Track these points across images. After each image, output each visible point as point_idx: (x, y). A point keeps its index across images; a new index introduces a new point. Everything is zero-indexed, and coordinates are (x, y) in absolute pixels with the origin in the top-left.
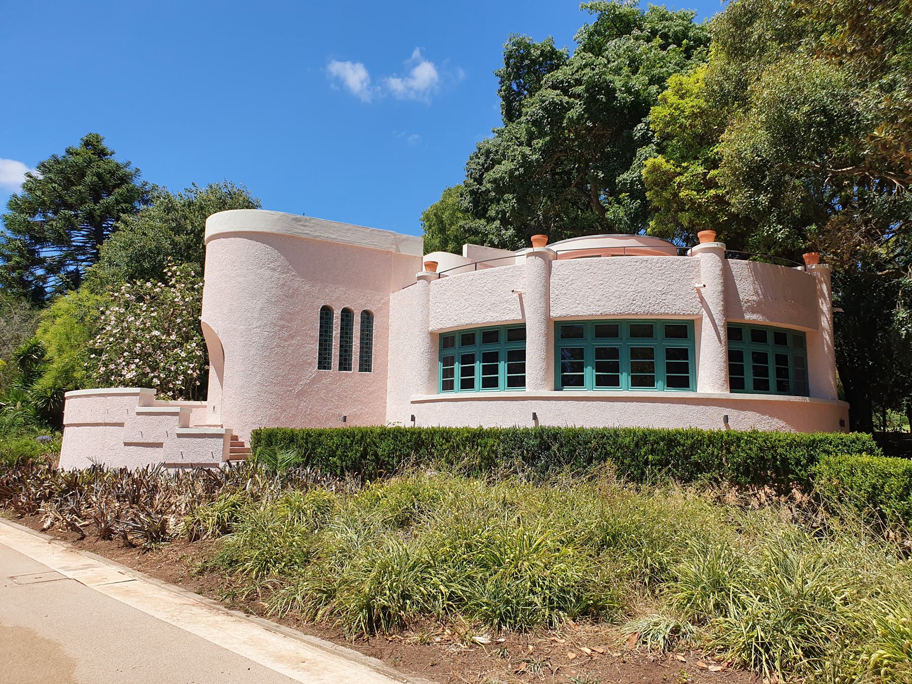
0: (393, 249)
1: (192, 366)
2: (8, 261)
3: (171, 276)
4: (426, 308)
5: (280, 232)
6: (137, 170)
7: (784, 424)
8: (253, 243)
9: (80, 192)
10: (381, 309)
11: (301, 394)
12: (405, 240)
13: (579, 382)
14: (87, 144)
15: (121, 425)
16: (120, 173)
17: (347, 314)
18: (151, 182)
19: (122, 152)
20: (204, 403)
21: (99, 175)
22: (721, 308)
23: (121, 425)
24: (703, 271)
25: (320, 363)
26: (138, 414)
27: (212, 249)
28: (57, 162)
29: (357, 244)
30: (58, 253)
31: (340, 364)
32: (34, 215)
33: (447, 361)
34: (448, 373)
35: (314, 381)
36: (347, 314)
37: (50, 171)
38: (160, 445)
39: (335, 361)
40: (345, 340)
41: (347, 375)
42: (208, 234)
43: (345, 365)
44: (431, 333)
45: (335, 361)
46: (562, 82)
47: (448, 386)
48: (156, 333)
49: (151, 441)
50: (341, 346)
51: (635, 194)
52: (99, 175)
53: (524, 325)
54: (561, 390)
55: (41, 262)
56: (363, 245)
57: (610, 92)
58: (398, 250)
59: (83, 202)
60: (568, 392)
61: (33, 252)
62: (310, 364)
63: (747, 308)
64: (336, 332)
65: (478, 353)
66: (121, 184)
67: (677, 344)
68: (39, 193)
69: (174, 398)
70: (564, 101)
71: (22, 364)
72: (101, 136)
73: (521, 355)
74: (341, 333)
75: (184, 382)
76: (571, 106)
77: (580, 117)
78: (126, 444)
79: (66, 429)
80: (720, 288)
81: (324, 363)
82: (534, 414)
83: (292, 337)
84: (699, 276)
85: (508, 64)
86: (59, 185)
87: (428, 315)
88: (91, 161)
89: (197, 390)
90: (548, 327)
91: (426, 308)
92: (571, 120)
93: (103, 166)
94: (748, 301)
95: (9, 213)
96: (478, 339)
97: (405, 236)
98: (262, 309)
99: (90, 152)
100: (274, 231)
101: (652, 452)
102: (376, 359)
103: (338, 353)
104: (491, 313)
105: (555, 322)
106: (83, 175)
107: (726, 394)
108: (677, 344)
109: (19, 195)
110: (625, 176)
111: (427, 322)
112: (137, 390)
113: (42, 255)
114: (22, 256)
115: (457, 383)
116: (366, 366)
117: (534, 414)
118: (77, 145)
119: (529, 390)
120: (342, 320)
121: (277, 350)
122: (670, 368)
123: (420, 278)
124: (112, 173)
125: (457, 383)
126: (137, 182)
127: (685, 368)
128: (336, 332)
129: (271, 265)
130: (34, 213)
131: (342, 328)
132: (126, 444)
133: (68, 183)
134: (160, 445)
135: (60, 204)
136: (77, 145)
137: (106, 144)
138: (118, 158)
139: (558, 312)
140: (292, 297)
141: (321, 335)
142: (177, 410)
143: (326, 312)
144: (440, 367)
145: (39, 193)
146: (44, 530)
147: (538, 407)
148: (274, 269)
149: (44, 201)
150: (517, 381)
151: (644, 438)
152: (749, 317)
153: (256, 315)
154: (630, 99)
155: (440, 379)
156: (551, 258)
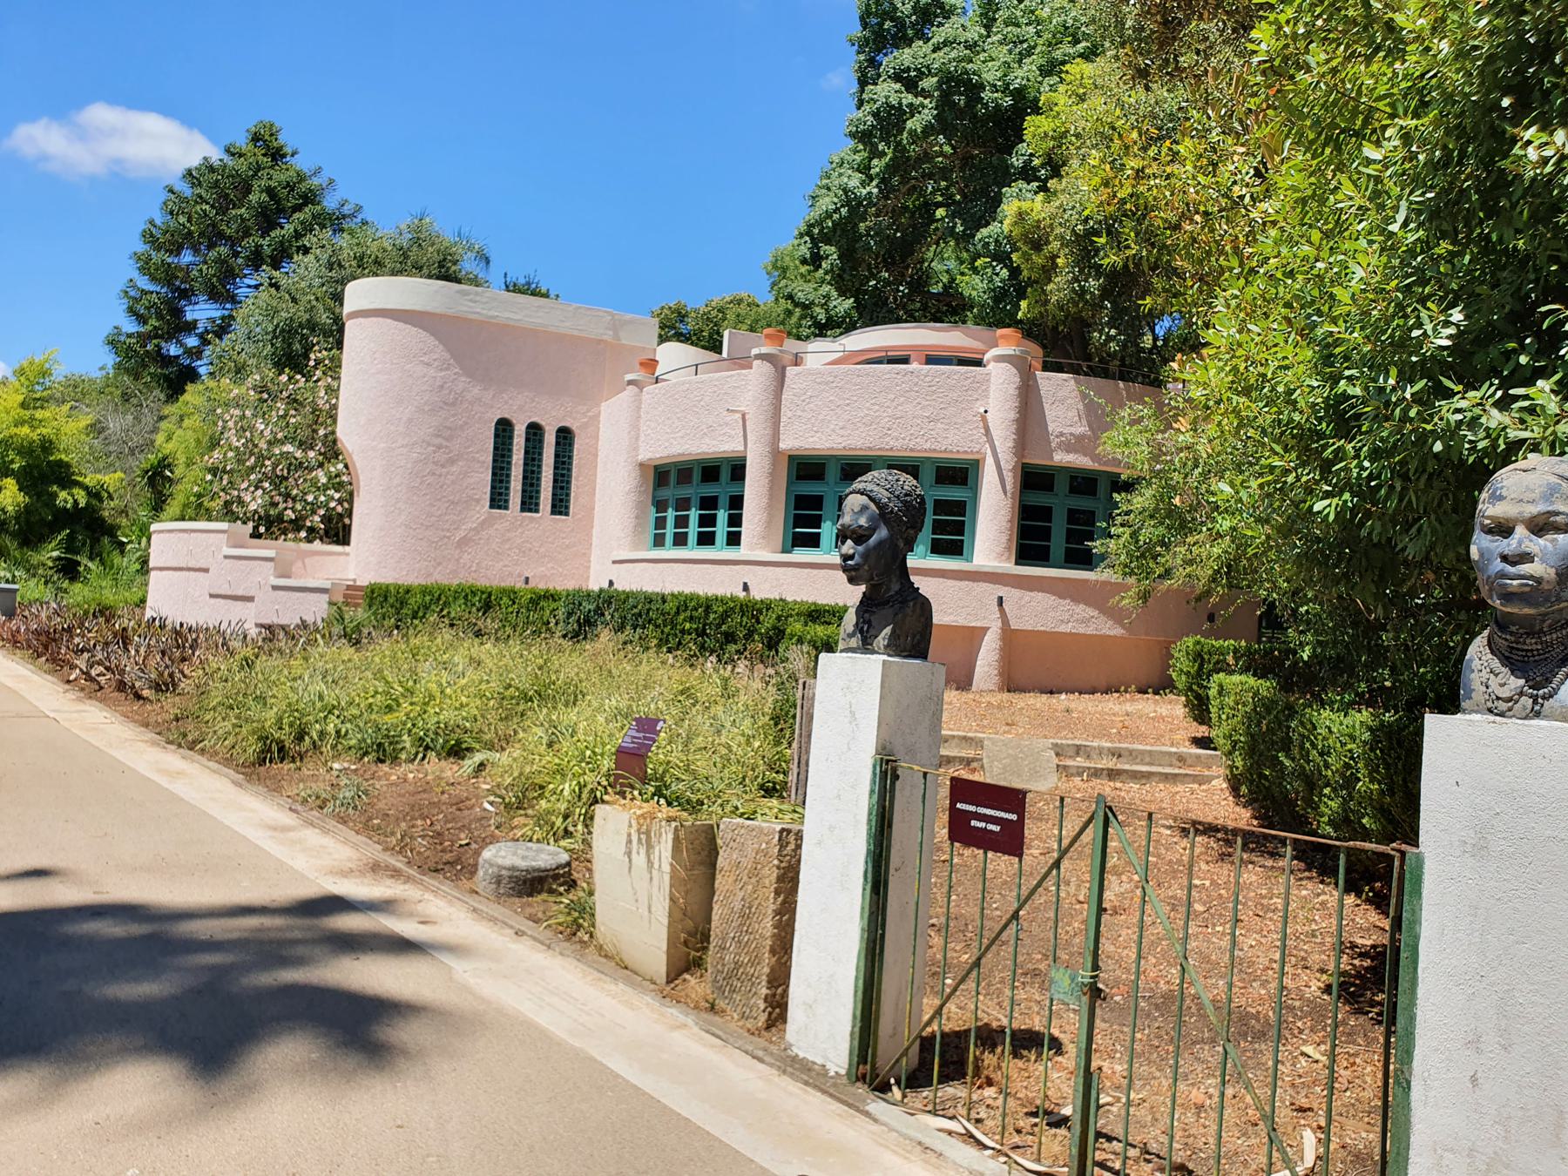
0: (608, 336)
1: (337, 496)
2: (145, 323)
3: (316, 367)
4: (635, 426)
5: (438, 311)
6: (331, 181)
7: (1096, 613)
8: (401, 325)
9: (243, 220)
10: (584, 426)
11: (464, 542)
12: (631, 322)
13: (813, 542)
14: (256, 138)
15: (206, 570)
16: (303, 187)
17: (535, 431)
18: (354, 199)
19: (309, 155)
20: (339, 548)
21: (270, 191)
22: (1011, 444)
23: (206, 570)
24: (993, 387)
25: (492, 500)
26: (226, 557)
27: (350, 327)
28: (212, 169)
29: (551, 329)
30: (218, 314)
31: (523, 503)
32: (179, 254)
33: (660, 506)
34: (660, 523)
35: (483, 525)
36: (535, 431)
37: (200, 184)
38: (250, 599)
39: (515, 497)
40: (533, 469)
41: (501, 517)
42: (348, 308)
43: (530, 503)
44: (641, 465)
45: (515, 497)
46: (908, 69)
47: (659, 541)
48: (288, 448)
49: (240, 593)
50: (525, 478)
51: (1001, 257)
52: (270, 191)
53: (744, 459)
54: (790, 552)
55: (191, 327)
56: (562, 331)
57: (975, 90)
58: (616, 336)
59: (247, 234)
60: (802, 555)
61: (178, 313)
62: (478, 501)
63: (1059, 446)
64: (518, 457)
65: (695, 494)
66: (305, 204)
67: (953, 493)
68: (182, 219)
69: (309, 540)
70: (904, 102)
71: (152, 482)
72: (278, 125)
73: (737, 502)
74: (525, 459)
75: (324, 519)
76: (914, 110)
77: (928, 130)
78: (212, 596)
79: (153, 574)
80: (1013, 415)
81: (498, 499)
82: (745, 584)
83: (452, 462)
84: (987, 397)
85: (865, 25)
86: (212, 207)
87: (637, 439)
88: (259, 168)
89: (337, 531)
90: (774, 464)
91: (635, 426)
92: (912, 133)
93: (279, 177)
94: (1062, 434)
95: (141, 247)
96: (697, 476)
97: (629, 316)
98: (410, 420)
99: (260, 152)
100: (429, 309)
101: (691, 618)
102: (576, 499)
103: (520, 488)
104: (707, 440)
105: (791, 458)
106: (248, 190)
107: (1009, 566)
108: (953, 493)
109: (158, 222)
110: (984, 232)
111: (636, 449)
112: (224, 526)
113: (189, 317)
114: (160, 317)
115: (669, 539)
116: (560, 505)
117: (745, 584)
118: (242, 141)
119: (743, 552)
120: (527, 440)
121: (430, 479)
122: (938, 527)
123: (630, 383)
124: (290, 187)
125: (669, 539)
126: (330, 203)
127: (959, 528)
128: (518, 457)
129: (425, 359)
130: (177, 250)
131: (526, 452)
132: (212, 596)
133: (224, 204)
134: (250, 599)
135: (214, 236)
136: (242, 141)
137: (286, 139)
138: (302, 163)
139: (788, 443)
140: (453, 404)
141: (494, 461)
142: (270, 553)
143: (504, 429)
144: (652, 513)
145: (182, 219)
146: (68, 682)
147: (747, 574)
148: (428, 364)
149: (190, 233)
150: (734, 540)
151: (686, 604)
152: (1061, 458)
153: (401, 429)
154: (1008, 101)
155: (651, 530)
156: (786, 362)
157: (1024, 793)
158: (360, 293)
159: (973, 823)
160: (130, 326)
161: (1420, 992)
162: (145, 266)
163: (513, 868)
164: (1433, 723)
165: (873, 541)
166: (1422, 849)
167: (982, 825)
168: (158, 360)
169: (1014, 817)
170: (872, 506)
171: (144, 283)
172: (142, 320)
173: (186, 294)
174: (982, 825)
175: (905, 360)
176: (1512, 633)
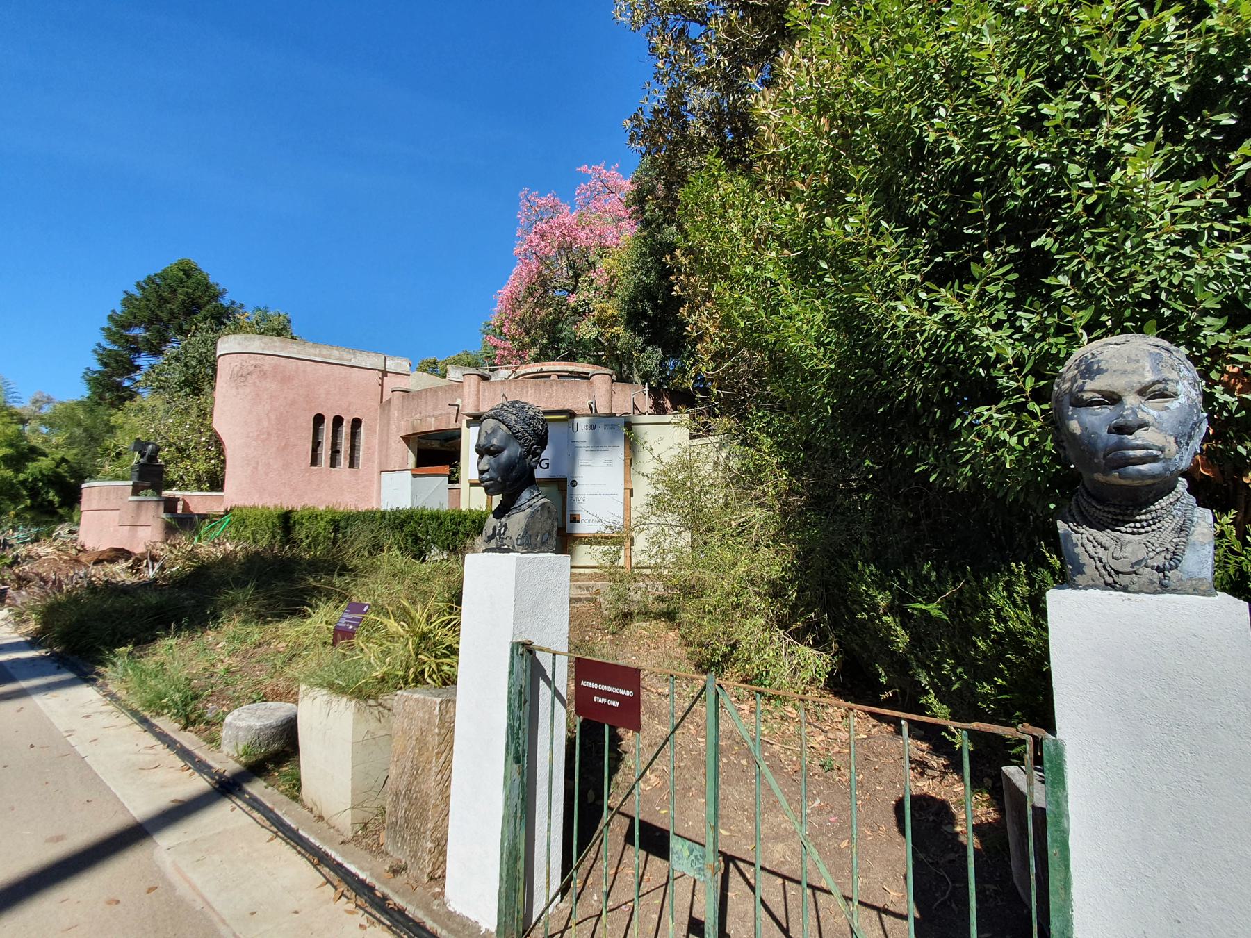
36: (338, 421)
81: (315, 461)
95: (107, 324)
157: (637, 671)
158: (227, 344)
159: (596, 699)
160: (98, 367)
161: (1075, 891)
162: (109, 333)
163: (250, 728)
164: (1055, 599)
165: (505, 455)
166: (1058, 735)
167: (603, 700)
168: (112, 385)
169: (630, 694)
170: (503, 427)
171: (107, 345)
172: (105, 365)
173: (138, 351)
174: (603, 700)
175: (631, 491)
176: (1114, 506)
